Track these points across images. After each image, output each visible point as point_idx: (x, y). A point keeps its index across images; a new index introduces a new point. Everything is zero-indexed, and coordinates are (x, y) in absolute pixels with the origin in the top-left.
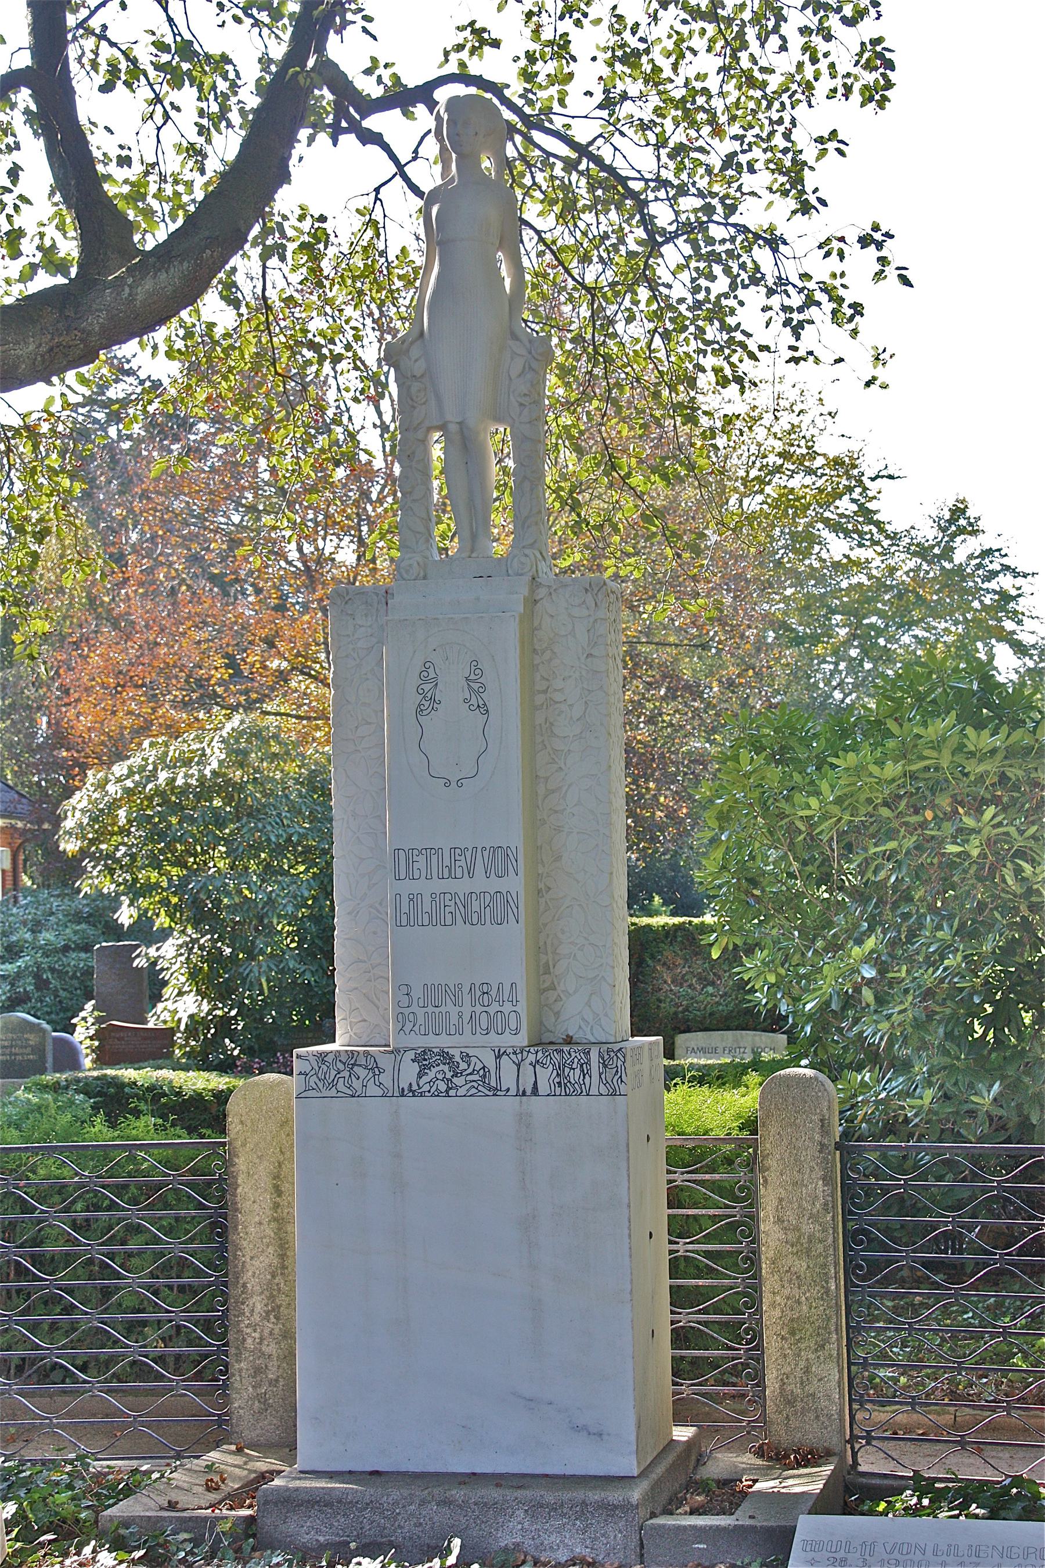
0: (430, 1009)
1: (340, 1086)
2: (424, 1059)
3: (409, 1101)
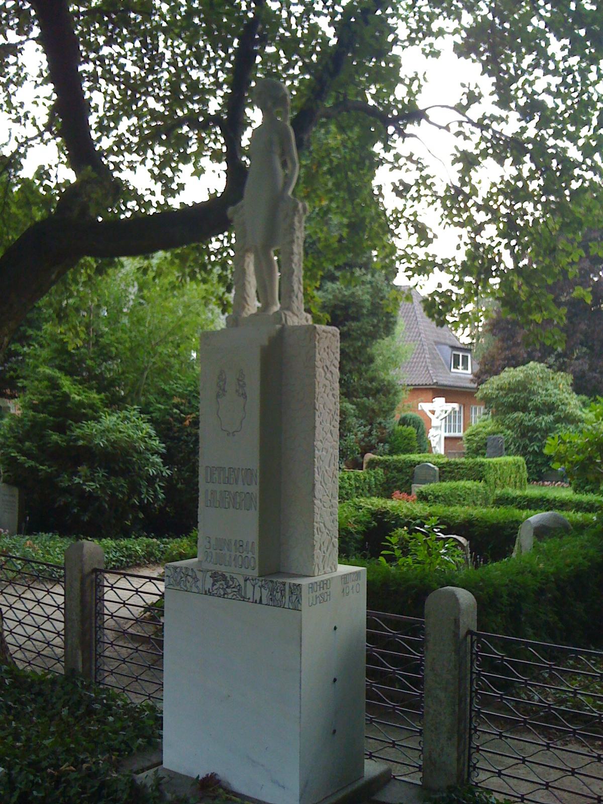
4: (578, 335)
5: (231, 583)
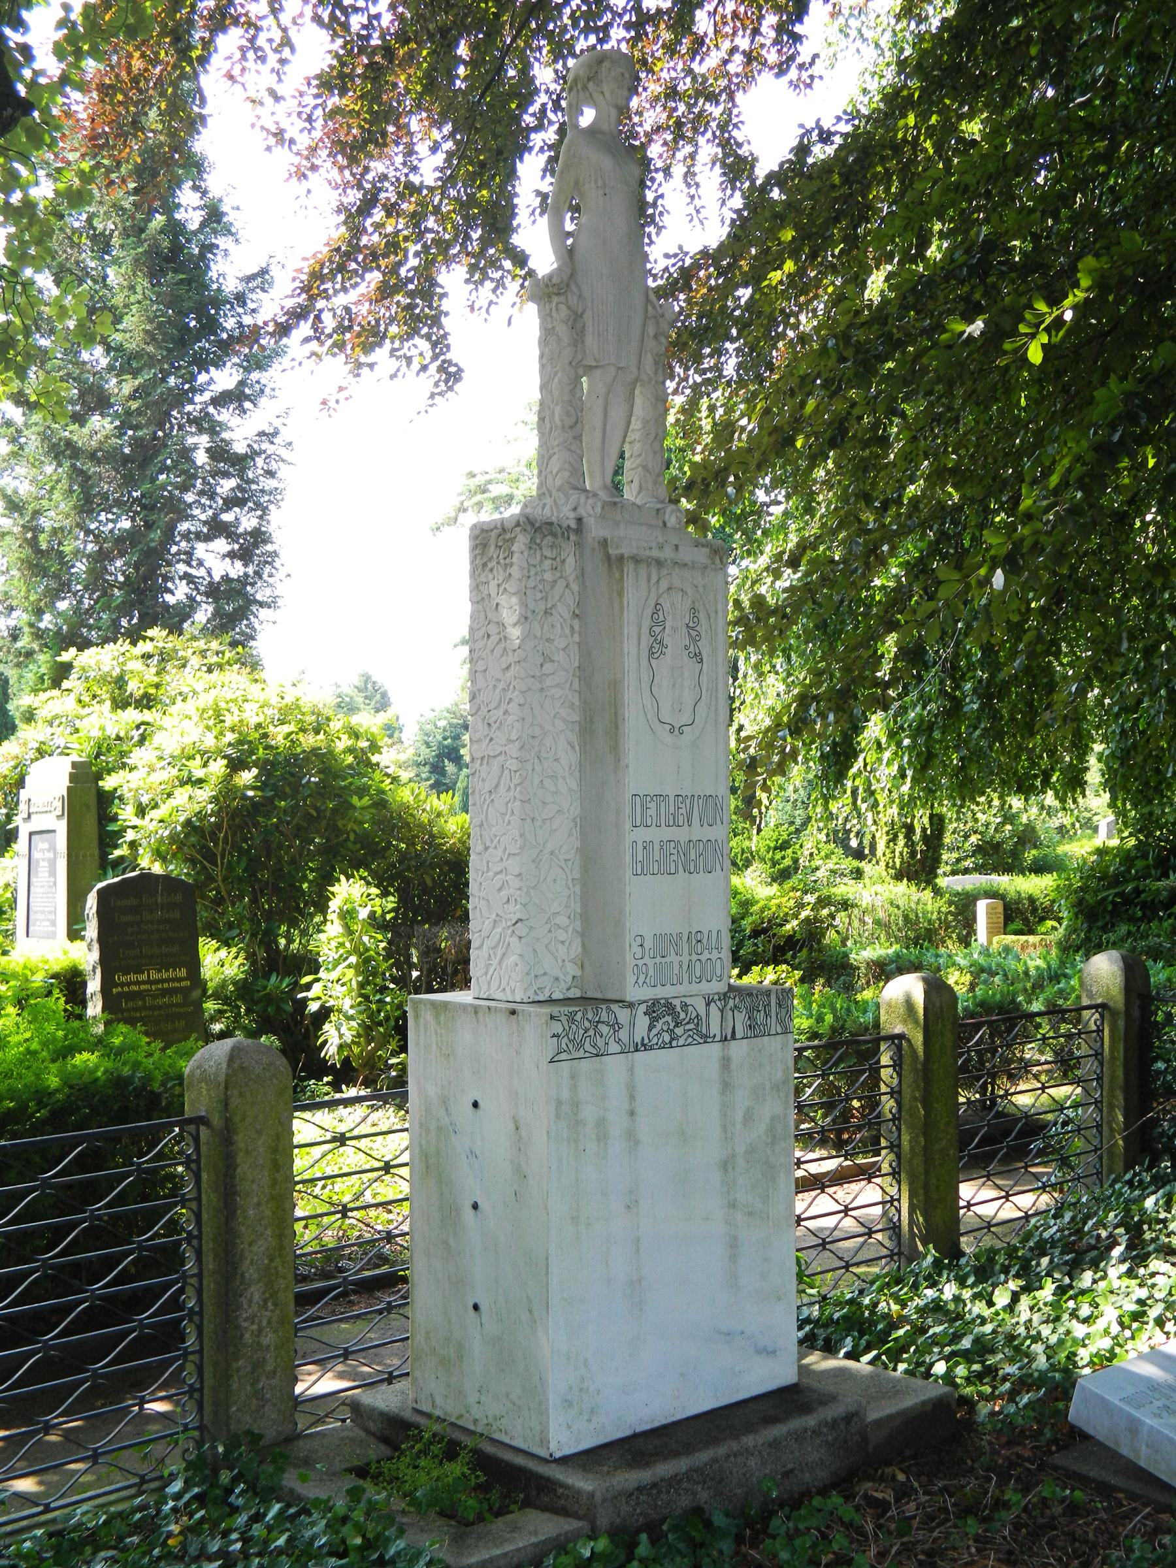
0: (658, 960)
1: (587, 1046)
3: (640, 1056)
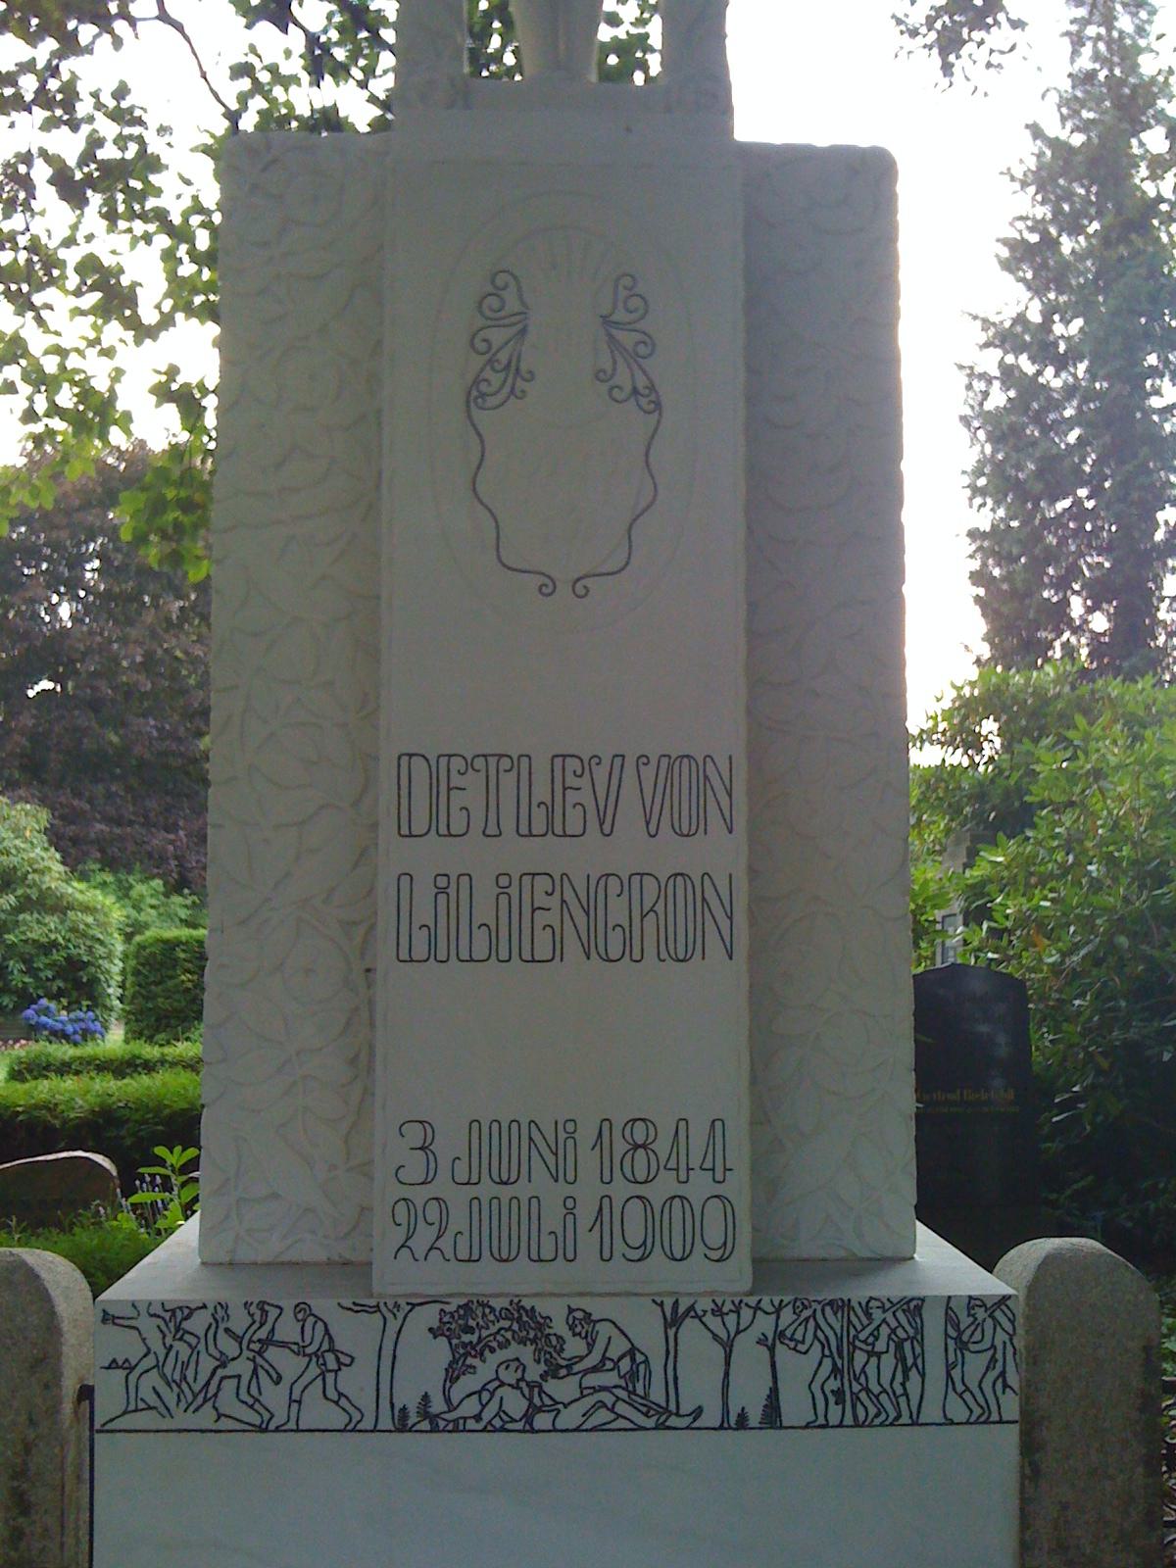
2: (465, 1329)
4: (17, 737)
5: (574, 1347)
